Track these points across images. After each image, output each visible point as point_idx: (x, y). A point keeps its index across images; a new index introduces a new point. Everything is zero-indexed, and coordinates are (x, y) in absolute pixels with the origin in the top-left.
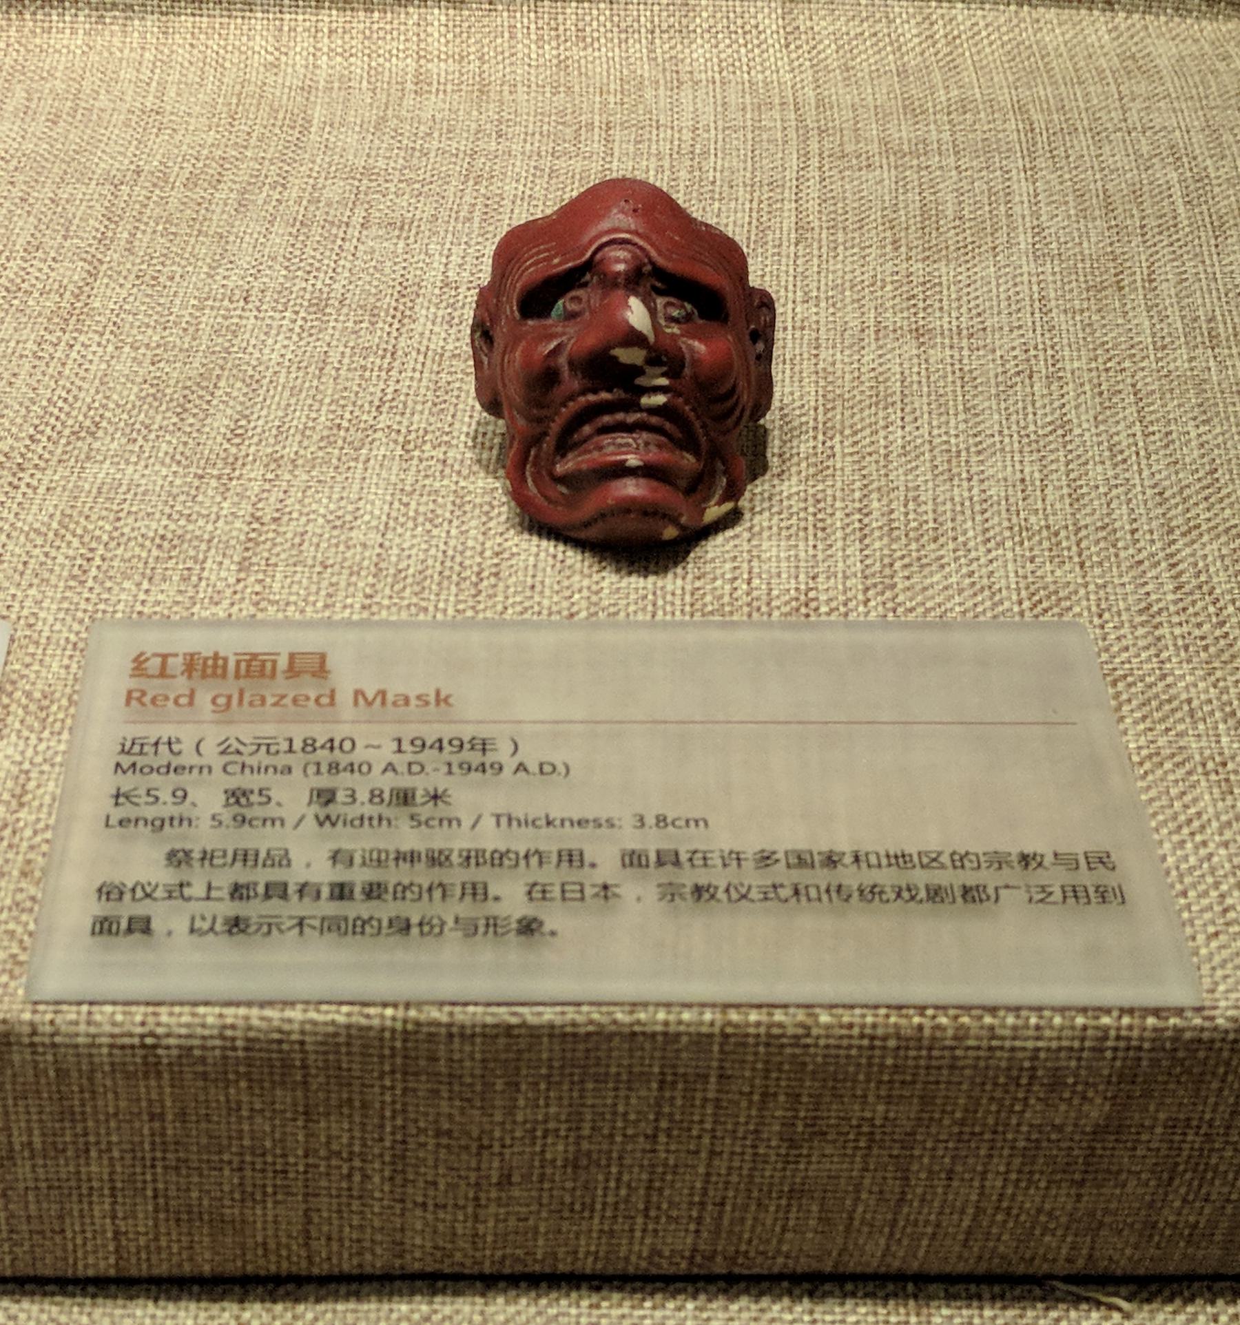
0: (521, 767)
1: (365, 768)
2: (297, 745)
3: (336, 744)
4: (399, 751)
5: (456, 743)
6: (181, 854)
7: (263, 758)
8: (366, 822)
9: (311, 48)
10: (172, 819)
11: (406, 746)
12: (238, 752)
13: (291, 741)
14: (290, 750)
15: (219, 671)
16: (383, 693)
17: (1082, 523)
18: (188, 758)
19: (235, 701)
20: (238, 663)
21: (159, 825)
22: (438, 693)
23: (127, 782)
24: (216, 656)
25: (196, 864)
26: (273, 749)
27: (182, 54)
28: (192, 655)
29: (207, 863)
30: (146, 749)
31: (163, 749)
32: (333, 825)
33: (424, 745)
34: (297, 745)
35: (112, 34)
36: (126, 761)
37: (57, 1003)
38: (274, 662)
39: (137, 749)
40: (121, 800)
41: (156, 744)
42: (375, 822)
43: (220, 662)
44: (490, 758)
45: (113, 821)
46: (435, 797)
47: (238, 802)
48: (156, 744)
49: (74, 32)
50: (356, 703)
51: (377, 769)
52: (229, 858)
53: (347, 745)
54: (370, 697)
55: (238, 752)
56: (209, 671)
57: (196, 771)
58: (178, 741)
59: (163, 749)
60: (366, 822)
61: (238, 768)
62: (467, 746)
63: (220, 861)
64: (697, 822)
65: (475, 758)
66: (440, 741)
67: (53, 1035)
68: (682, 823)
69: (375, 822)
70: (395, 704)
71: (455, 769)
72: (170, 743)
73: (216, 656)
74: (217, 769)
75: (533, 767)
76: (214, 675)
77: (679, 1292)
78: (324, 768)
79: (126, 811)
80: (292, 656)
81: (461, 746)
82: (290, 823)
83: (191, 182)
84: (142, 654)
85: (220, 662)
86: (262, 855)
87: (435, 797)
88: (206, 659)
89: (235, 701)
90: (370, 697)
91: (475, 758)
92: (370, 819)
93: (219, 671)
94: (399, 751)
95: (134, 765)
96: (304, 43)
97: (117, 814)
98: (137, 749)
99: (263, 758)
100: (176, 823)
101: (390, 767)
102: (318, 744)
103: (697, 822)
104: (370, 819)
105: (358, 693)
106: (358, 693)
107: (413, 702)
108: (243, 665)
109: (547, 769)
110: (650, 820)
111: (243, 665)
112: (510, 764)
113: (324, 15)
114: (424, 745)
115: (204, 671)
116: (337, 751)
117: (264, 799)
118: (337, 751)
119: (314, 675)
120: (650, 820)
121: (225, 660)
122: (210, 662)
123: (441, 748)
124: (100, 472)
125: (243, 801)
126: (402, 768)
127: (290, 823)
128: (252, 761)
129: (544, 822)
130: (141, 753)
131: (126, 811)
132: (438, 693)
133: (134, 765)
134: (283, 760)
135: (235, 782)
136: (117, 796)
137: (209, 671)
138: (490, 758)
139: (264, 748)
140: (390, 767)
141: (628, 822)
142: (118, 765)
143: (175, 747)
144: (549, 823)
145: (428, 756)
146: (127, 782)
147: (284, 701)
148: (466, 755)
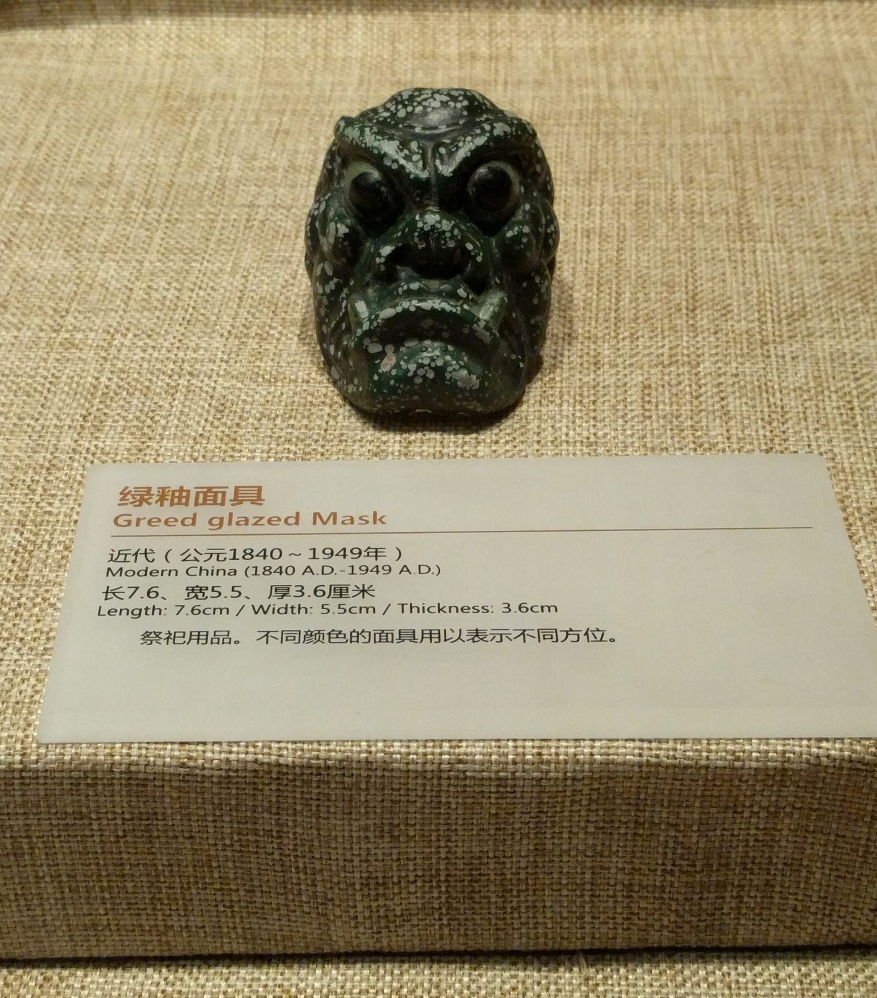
0: (405, 569)
1: (290, 571)
2: (240, 554)
3: (268, 553)
4: (314, 558)
5: (356, 551)
6: (153, 635)
7: (213, 563)
8: (289, 610)
9: (683, 32)
10: (147, 609)
11: (319, 554)
12: (196, 560)
13: (235, 550)
14: (234, 558)
15: (184, 501)
16: (334, 515)
17: (703, 381)
18: (159, 564)
19: (226, 521)
20: (198, 493)
21: (137, 614)
22: (375, 514)
23: (113, 582)
24: (181, 489)
25: (163, 642)
26: (221, 557)
27: (726, 36)
28: (164, 489)
29: (171, 641)
30: (129, 558)
31: (141, 558)
32: (265, 613)
33: (332, 553)
34: (240, 554)
35: (671, 23)
36: (115, 567)
37: (785, 739)
38: (224, 494)
39: (122, 558)
40: (110, 595)
41: (136, 554)
42: (296, 611)
43: (184, 494)
44: (381, 562)
45: (104, 611)
46: (364, 591)
47: (196, 596)
48: (136, 554)
49: (642, 21)
50: (315, 523)
51: (300, 570)
52: (187, 639)
53: (276, 554)
54: (325, 519)
55: (196, 560)
56: (176, 501)
57: (166, 573)
58: (152, 552)
59: (141, 558)
60: (289, 610)
61: (197, 571)
62: (364, 554)
63: (181, 640)
64: (221, 610)
65: (371, 562)
66: (344, 549)
67: (22, 771)
68: (357, 610)
69: (296, 611)
70: (238, 523)
71: (356, 570)
72: (146, 554)
73: (181, 489)
74: (182, 572)
75: (414, 569)
76: (179, 503)
77: (418, 962)
78: (260, 571)
79: (114, 603)
80: (237, 489)
81: (360, 553)
82: (380, 610)
83: (781, 129)
84: (126, 488)
85: (184, 494)
86: (211, 635)
87: (364, 591)
88: (174, 492)
89: (226, 521)
90: (325, 519)
91: (371, 562)
92: (292, 608)
93: (184, 501)
94: (314, 558)
95: (121, 569)
96: (816, 27)
97: (107, 606)
98: (122, 558)
99: (213, 563)
100: (150, 612)
101: (308, 570)
102: (254, 554)
103: (221, 610)
104: (292, 608)
105: (316, 515)
106: (316, 515)
107: (357, 521)
108: (201, 496)
109: (424, 569)
110: (514, 607)
111: (201, 496)
112: (397, 567)
113: (800, 7)
114: (332, 553)
115: (172, 501)
116: (268, 558)
117: (237, 594)
118: (268, 558)
119: (253, 502)
120: (514, 607)
121: (188, 492)
122: (177, 494)
123: (345, 556)
124: (824, 346)
125: (200, 595)
126: (317, 569)
127: (380, 610)
128: (207, 566)
129: (436, 609)
130: (125, 561)
131: (114, 603)
132: (375, 514)
133: (121, 569)
134: (228, 565)
135: (193, 582)
136: (107, 593)
137: (176, 501)
138: (381, 562)
139: (215, 556)
140: (308, 570)
141: (500, 608)
142: (109, 569)
143: (150, 557)
144: (440, 610)
145: (336, 562)
146: (113, 582)
147: (261, 522)
148: (364, 561)
